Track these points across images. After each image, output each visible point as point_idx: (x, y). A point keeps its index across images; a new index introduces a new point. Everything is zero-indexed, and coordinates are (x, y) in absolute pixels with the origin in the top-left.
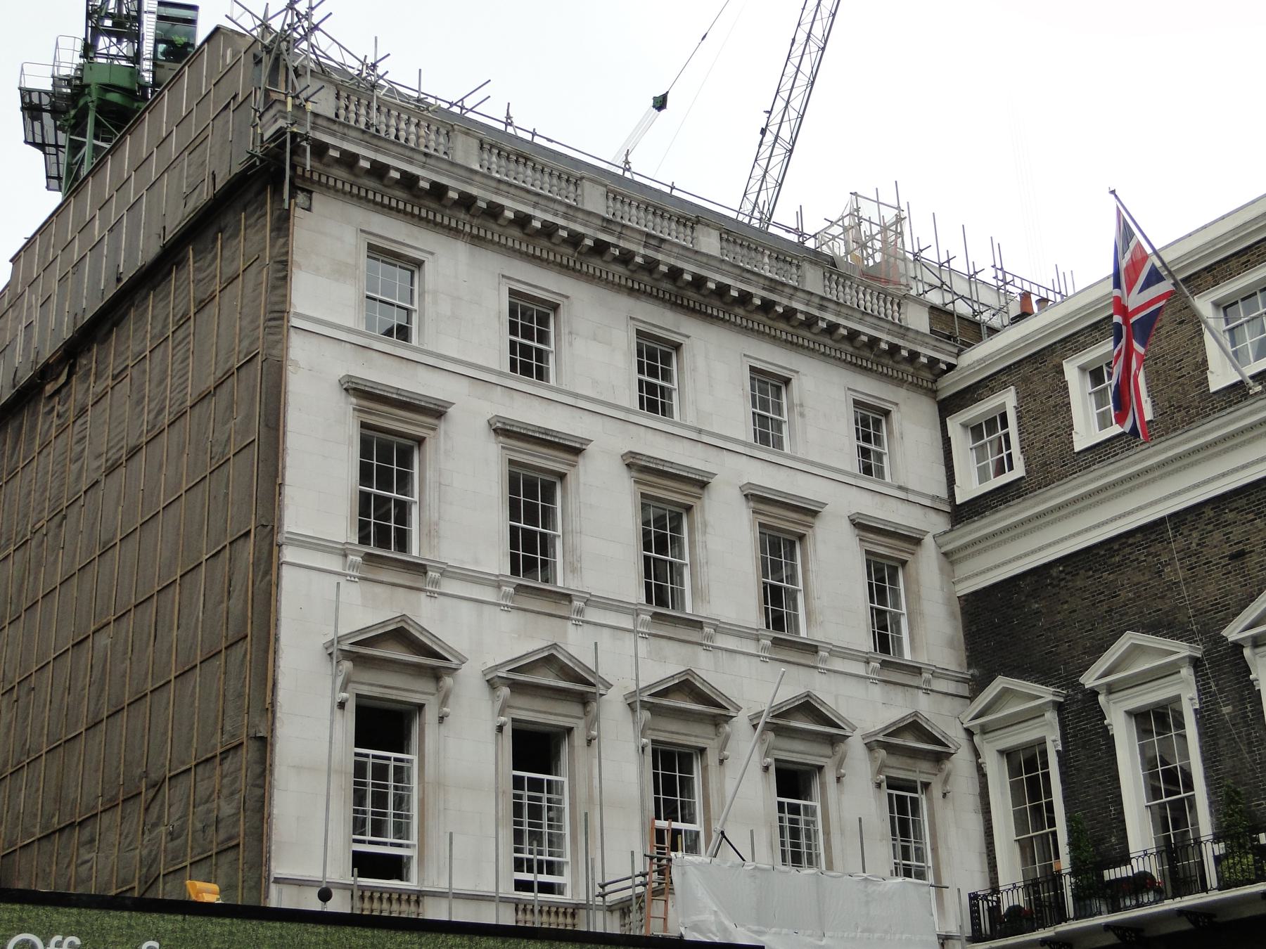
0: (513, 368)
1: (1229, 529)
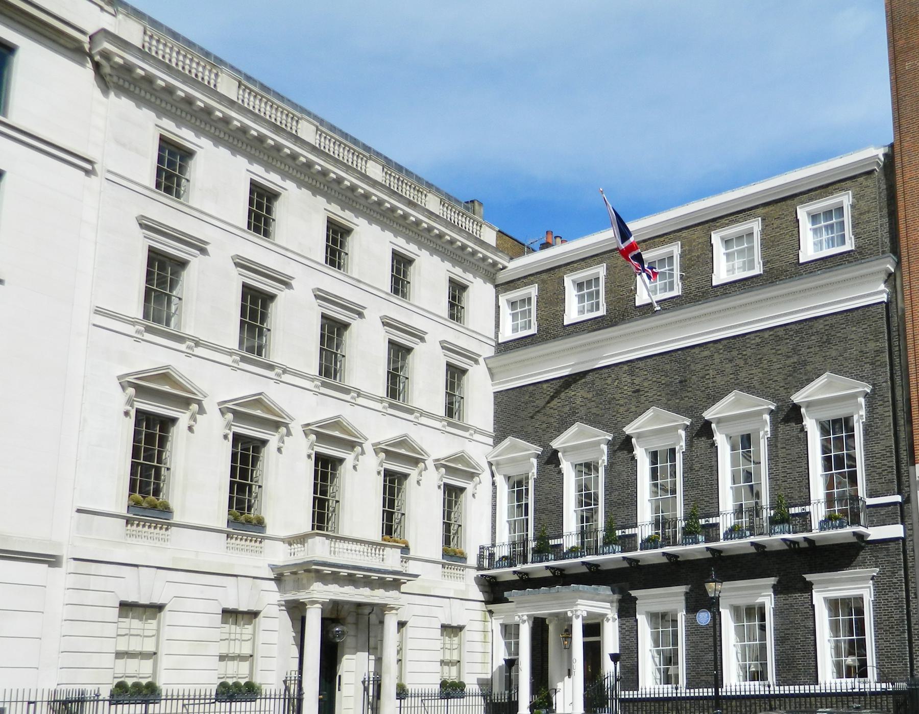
0: (249, 227)
1: (634, 377)
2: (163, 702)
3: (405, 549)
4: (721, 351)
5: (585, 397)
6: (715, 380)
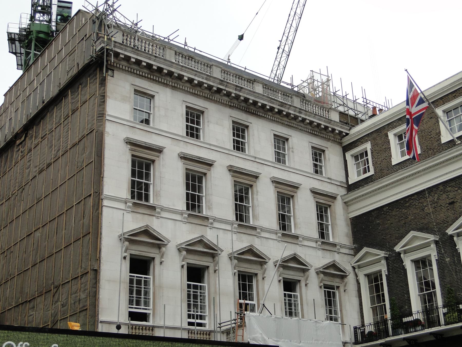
0: (187, 135)
1: (448, 194)
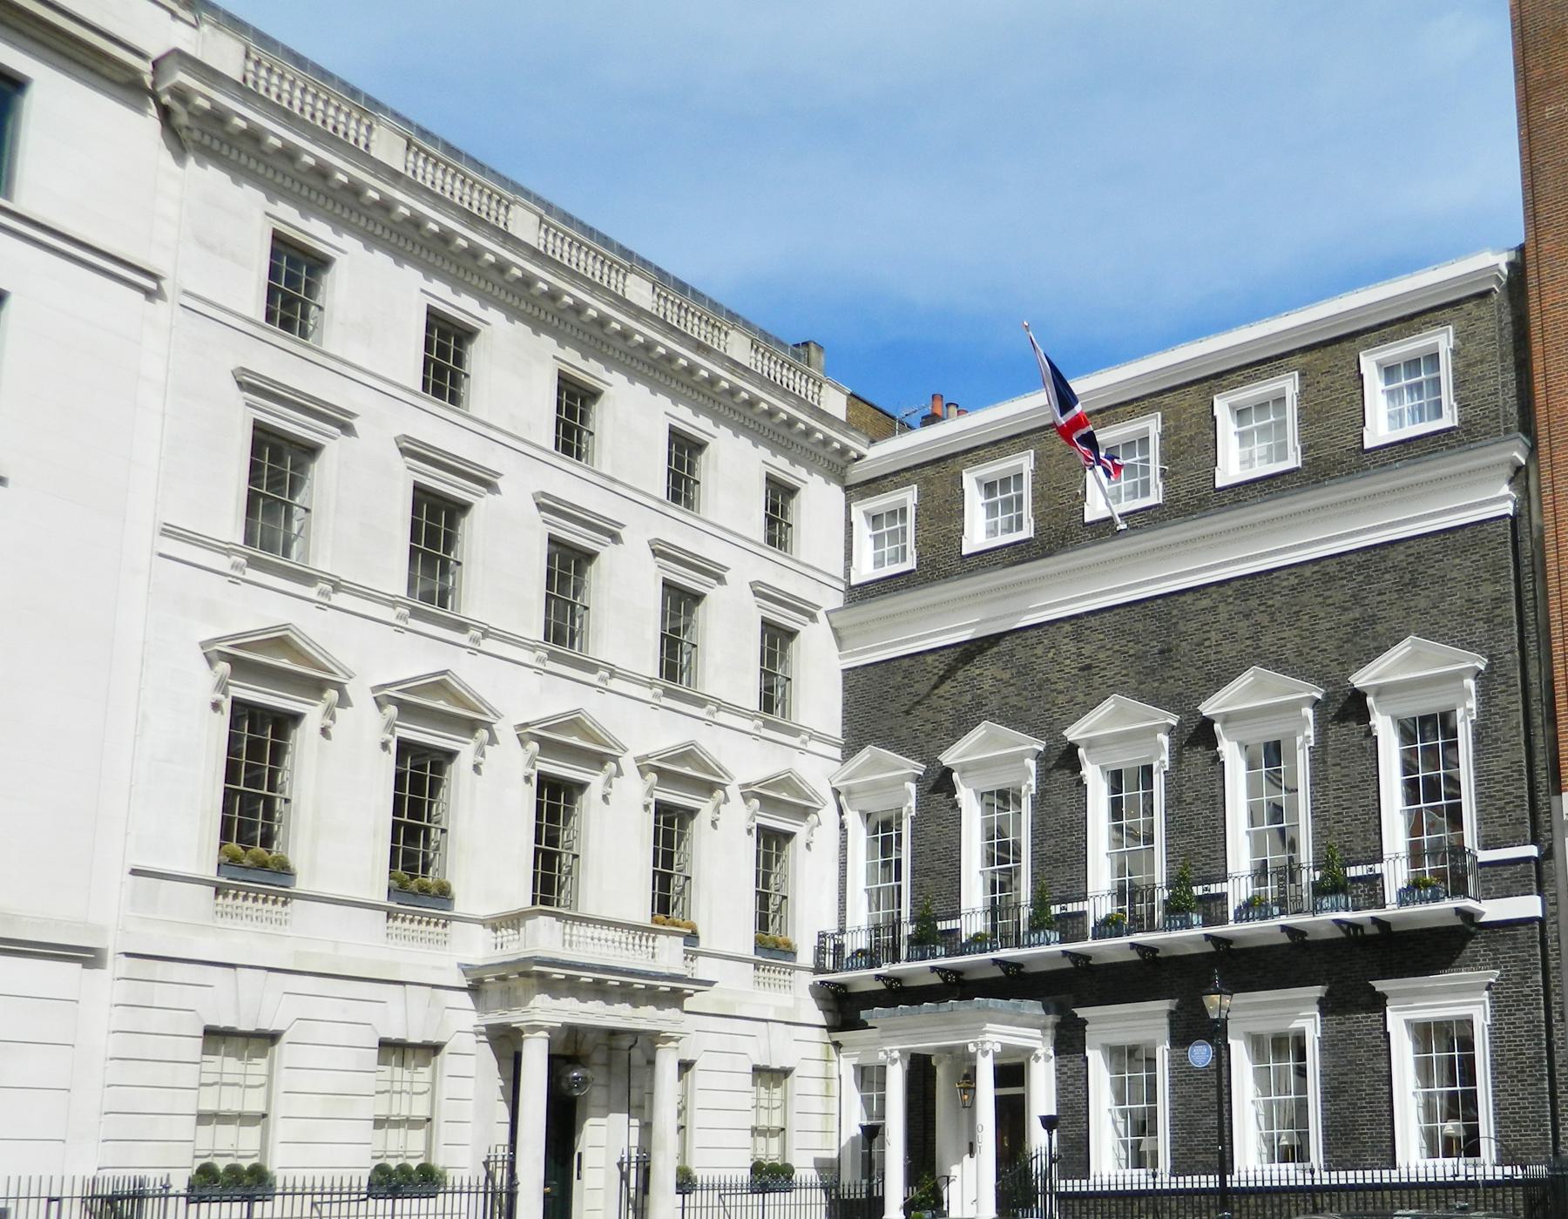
0: (425, 388)
1: (1081, 644)
2: (278, 1199)
3: (692, 937)
4: (1231, 600)
5: (999, 677)
6: (1220, 649)
